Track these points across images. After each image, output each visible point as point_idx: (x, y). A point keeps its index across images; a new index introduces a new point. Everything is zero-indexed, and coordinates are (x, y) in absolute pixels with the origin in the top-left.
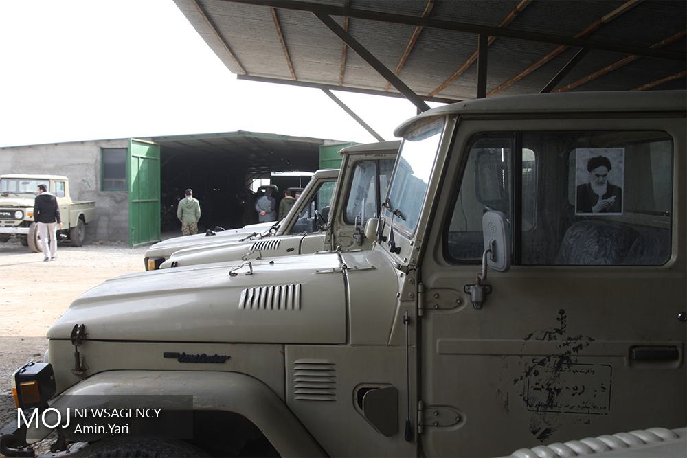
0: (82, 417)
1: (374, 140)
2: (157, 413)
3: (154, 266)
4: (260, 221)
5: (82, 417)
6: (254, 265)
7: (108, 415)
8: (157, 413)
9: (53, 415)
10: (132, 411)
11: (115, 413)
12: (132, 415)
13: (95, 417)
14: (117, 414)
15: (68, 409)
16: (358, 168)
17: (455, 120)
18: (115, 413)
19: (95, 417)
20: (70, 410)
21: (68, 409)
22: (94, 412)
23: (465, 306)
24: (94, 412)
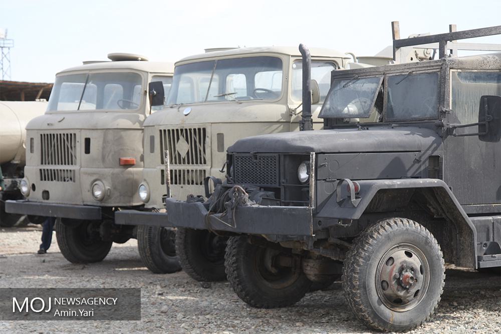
0: (60, 304)
1: (302, 106)
2: (115, 301)
3: (329, 114)
4: (152, 107)
5: (60, 304)
6: (58, 252)
7: (78, 303)
8: (115, 301)
9: (36, 302)
10: (96, 300)
11: (84, 301)
12: (96, 303)
13: (69, 304)
14: (85, 302)
15: (50, 298)
16: (297, 113)
17: (210, 193)
18: (84, 301)
19: (69, 304)
20: (51, 299)
21: (50, 298)
22: (69, 301)
23: (447, 187)
24: (69, 301)
